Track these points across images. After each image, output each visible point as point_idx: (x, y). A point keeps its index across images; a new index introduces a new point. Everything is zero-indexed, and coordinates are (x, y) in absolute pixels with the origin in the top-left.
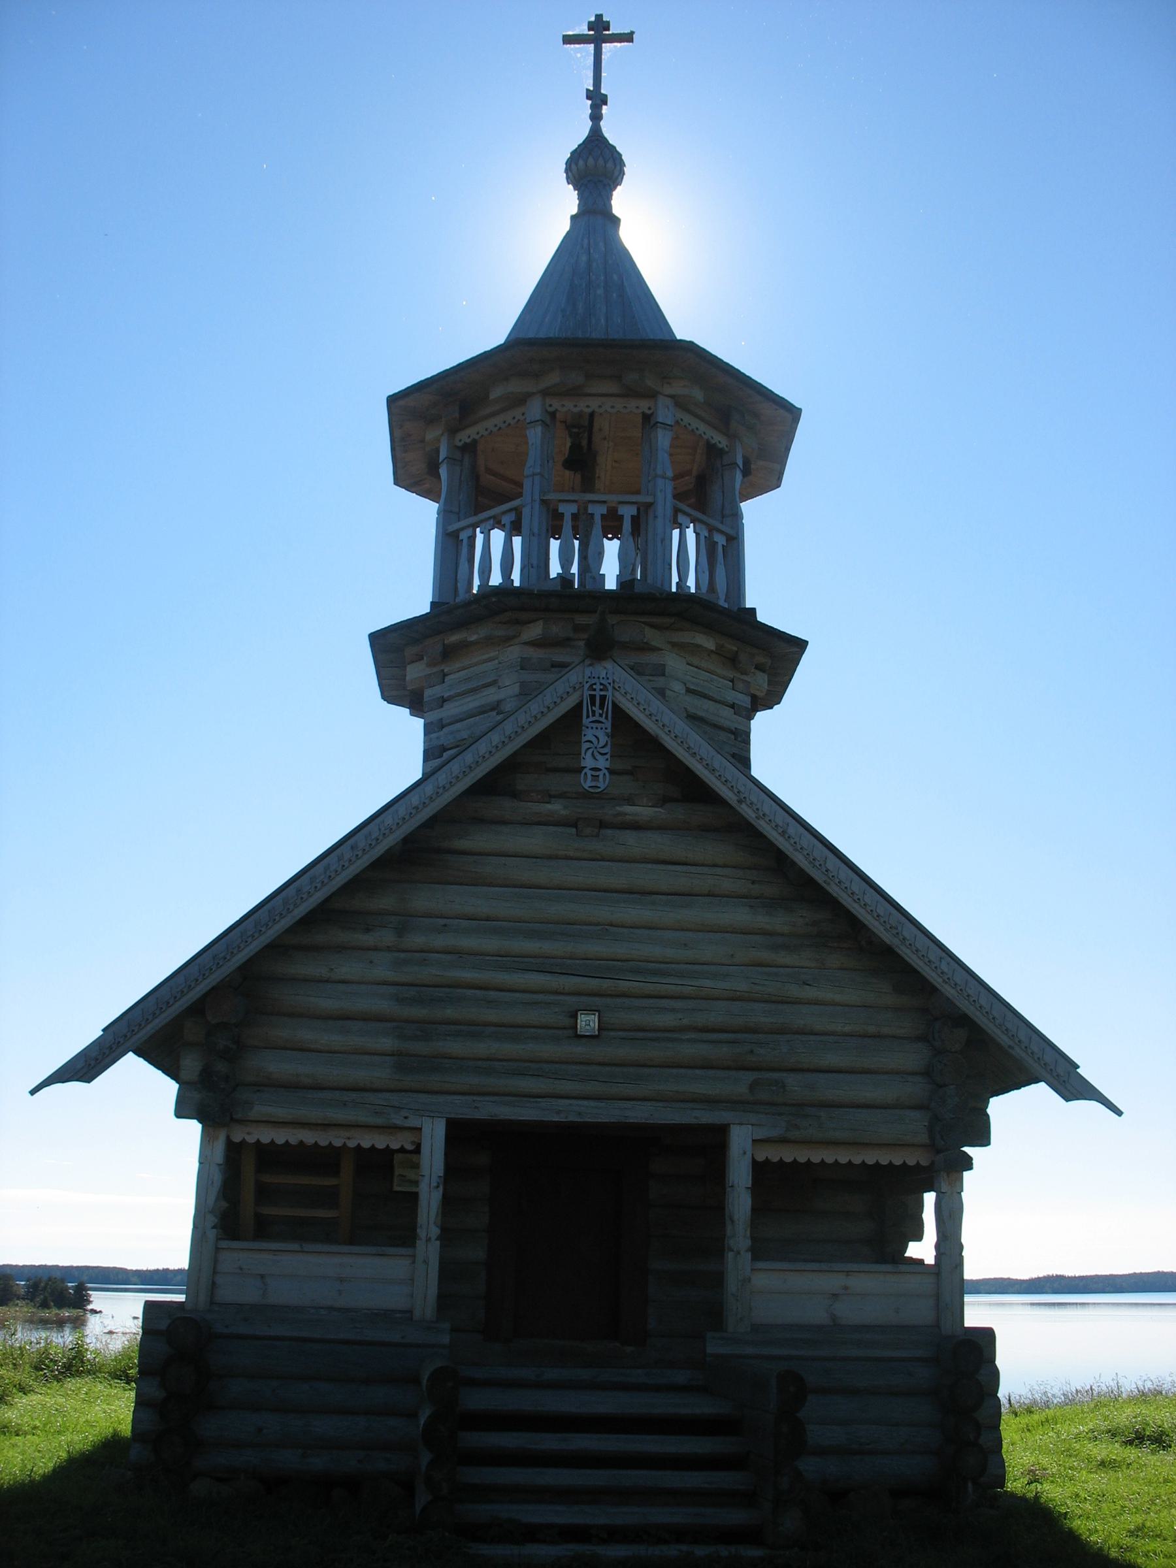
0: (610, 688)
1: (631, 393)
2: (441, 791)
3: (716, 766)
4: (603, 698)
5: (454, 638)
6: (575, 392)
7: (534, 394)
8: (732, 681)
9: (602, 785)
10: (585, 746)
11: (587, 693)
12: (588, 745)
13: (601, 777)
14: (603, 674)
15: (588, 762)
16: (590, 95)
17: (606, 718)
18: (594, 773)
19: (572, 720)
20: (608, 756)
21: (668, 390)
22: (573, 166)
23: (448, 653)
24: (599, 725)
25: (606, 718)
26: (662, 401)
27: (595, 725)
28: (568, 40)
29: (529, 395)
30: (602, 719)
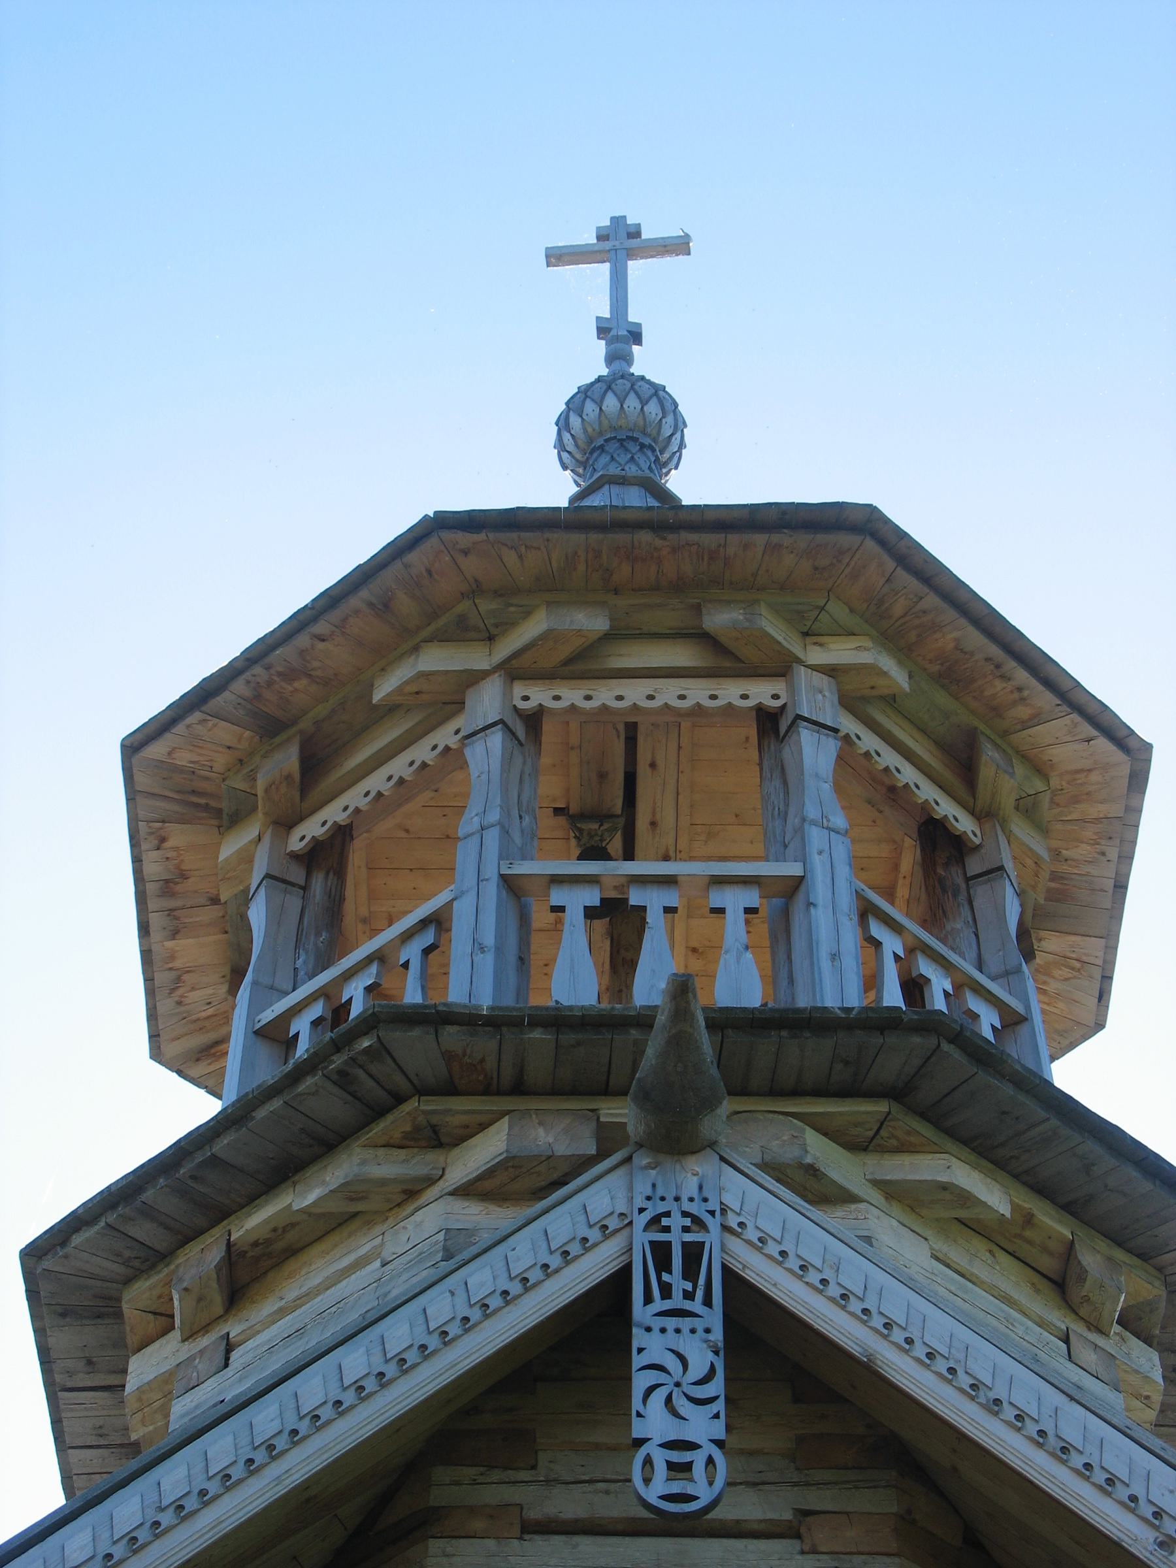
0: (713, 1224)
1: (726, 658)
2: (167, 1519)
3: (1072, 1435)
4: (693, 1253)
5: (253, 1223)
6: (581, 663)
7: (484, 675)
8: (1066, 1341)
9: (704, 1492)
10: (641, 1381)
11: (641, 1239)
12: (652, 1377)
13: (699, 1470)
14: (690, 1187)
15: (653, 1423)
16: (603, 330)
17: (708, 1302)
18: (677, 1457)
19: (603, 1316)
20: (719, 1406)
21: (817, 656)
22: (575, 421)
23: (243, 1278)
24: (685, 1323)
25: (708, 1302)
26: (802, 675)
27: (671, 1323)
28: (557, 257)
29: (474, 678)
30: (696, 1306)
